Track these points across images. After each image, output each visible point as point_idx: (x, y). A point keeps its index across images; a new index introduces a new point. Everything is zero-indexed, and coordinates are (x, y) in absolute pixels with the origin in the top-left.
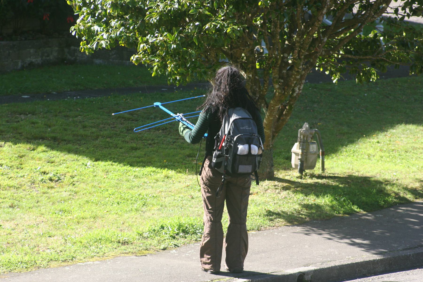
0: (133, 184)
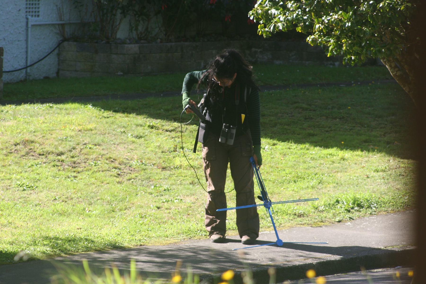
0: (310, 165)
